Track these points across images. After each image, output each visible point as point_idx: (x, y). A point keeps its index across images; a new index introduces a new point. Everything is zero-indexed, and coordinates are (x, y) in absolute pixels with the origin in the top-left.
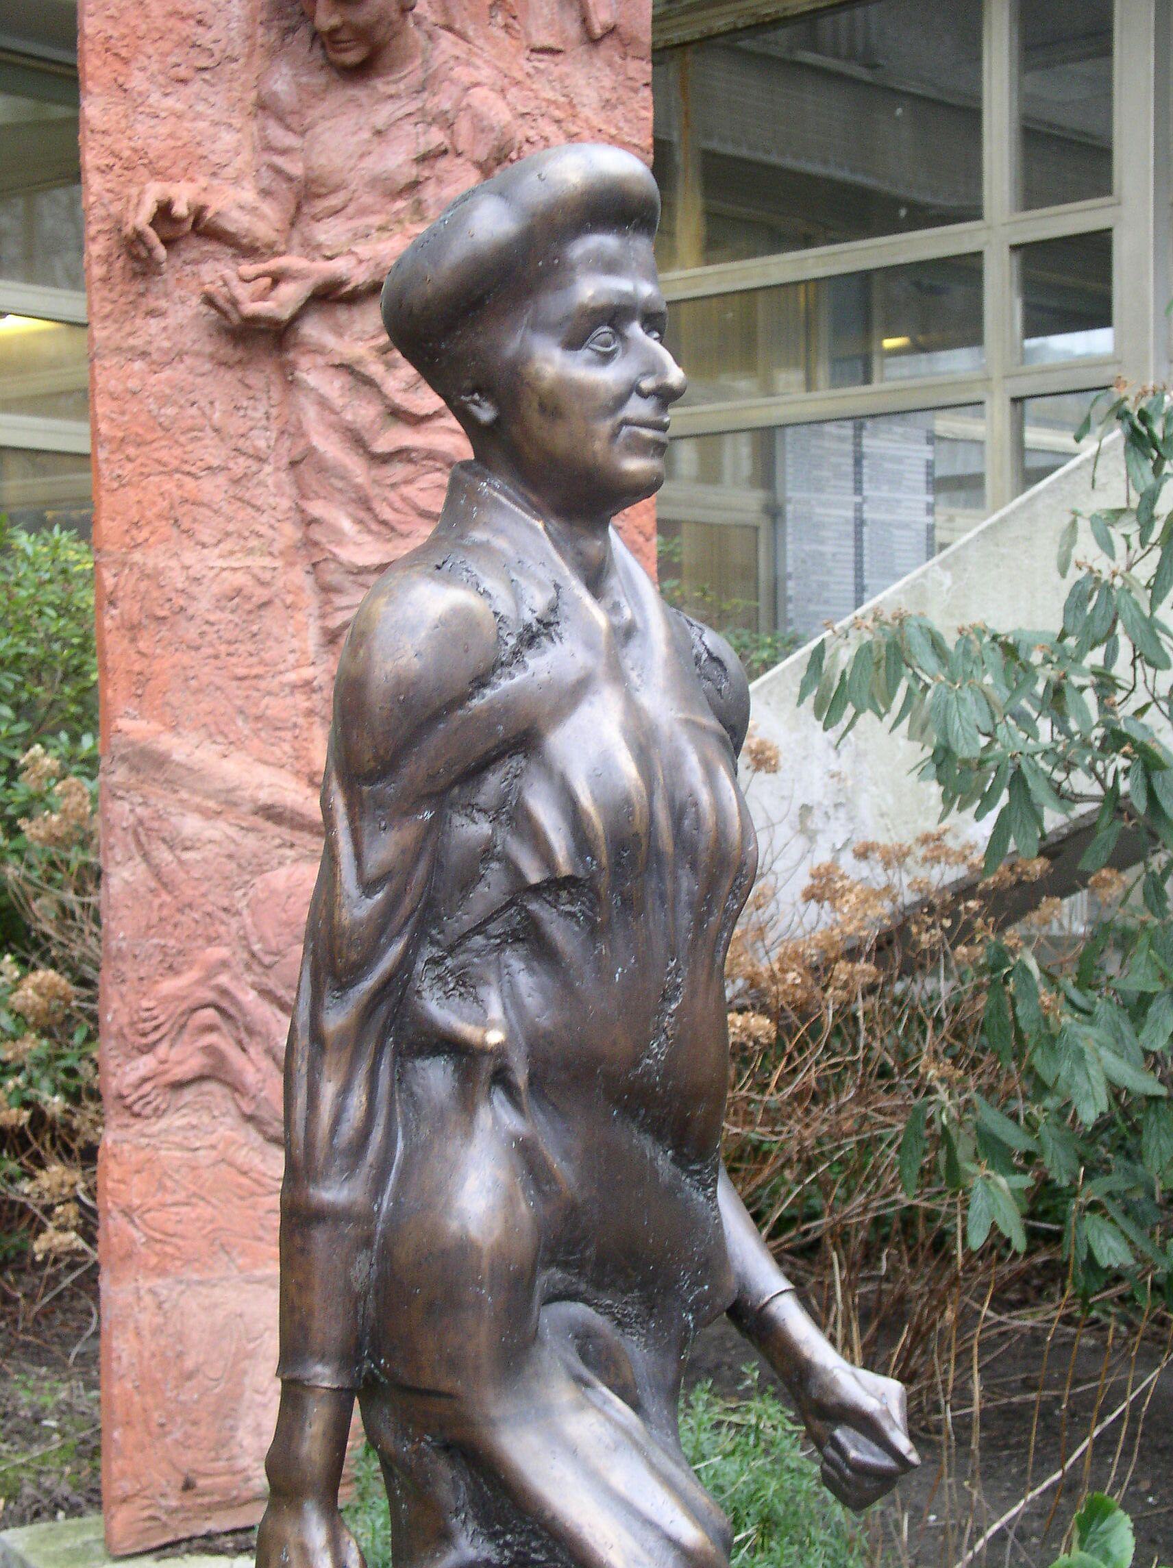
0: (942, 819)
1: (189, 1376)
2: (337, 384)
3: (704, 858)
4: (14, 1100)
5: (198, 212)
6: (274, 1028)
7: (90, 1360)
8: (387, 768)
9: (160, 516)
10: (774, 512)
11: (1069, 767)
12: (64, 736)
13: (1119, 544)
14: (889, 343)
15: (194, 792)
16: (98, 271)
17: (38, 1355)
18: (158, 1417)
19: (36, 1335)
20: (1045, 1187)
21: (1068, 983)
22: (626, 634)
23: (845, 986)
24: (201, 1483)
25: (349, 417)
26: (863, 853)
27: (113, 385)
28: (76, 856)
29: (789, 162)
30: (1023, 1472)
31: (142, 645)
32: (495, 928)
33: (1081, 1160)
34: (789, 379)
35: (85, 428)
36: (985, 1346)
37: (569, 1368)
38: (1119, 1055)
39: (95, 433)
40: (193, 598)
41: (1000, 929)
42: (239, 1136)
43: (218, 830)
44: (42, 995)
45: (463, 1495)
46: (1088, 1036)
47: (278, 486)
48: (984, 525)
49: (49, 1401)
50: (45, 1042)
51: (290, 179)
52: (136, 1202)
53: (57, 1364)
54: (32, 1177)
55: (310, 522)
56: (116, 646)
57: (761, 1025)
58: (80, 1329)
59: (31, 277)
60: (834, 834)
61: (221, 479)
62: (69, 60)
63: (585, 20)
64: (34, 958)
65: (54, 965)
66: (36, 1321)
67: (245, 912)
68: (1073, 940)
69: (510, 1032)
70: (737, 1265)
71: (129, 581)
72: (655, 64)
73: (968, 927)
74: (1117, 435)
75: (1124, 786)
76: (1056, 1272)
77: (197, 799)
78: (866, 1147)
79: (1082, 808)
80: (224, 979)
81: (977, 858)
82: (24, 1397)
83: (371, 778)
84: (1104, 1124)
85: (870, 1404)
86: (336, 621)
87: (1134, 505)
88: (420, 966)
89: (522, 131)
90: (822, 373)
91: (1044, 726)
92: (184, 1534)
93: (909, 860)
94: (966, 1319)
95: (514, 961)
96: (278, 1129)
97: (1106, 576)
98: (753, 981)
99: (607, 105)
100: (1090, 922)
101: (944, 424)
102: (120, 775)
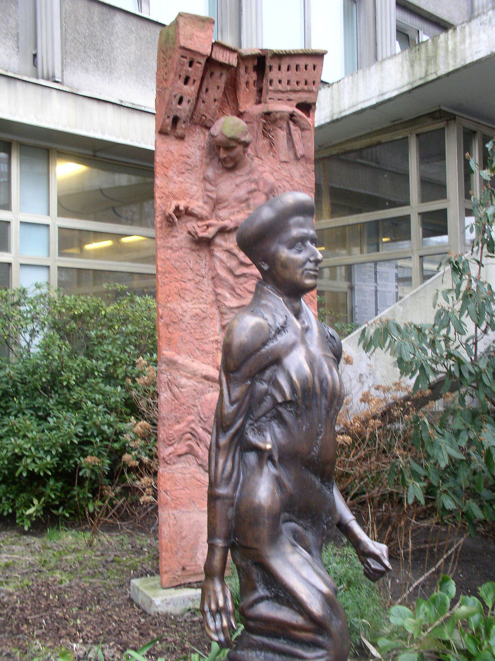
0: (400, 378)
1: (183, 538)
2: (225, 255)
3: (329, 395)
4: (135, 458)
5: (186, 209)
6: (207, 439)
7: (156, 532)
8: (237, 369)
9: (175, 293)
10: (352, 288)
11: (436, 363)
12: (148, 354)
13: (450, 299)
14: (384, 240)
15: (184, 371)
16: (158, 225)
17: (142, 530)
18: (175, 549)
19: (141, 524)
20: (430, 485)
21: (437, 427)
22: (306, 330)
23: (372, 427)
24: (187, 568)
25: (228, 264)
26: (377, 388)
27: (162, 257)
28: (152, 389)
29: (355, 190)
30: (424, 568)
31: (170, 330)
32: (268, 415)
33: (441, 478)
34: (356, 250)
35: (155, 267)
36: (413, 531)
37: (290, 542)
38: (451, 448)
39: (157, 269)
40: (184, 316)
41: (417, 410)
42: (197, 470)
43: (191, 382)
44: (142, 428)
45: (260, 577)
46: (443, 442)
47: (208, 284)
48: (412, 293)
49: (145, 544)
50: (143, 442)
51: (212, 198)
52: (168, 488)
53: (147, 533)
54: (140, 480)
55: (217, 294)
56: (162, 330)
57: (348, 439)
58: (153, 523)
59: (141, 225)
60: (369, 382)
61: (192, 283)
62: (151, 165)
63: (295, 154)
64: (140, 418)
65: (145, 420)
66: (141, 520)
67: (199, 407)
68: (438, 413)
69: (273, 445)
70: (339, 512)
71: (166, 311)
72: (315, 163)
73: (408, 409)
74: (449, 268)
75: (453, 369)
76: (434, 509)
77: (185, 374)
78: (378, 473)
79: (441, 375)
80: (193, 425)
81: (410, 389)
82: (138, 542)
83: (233, 372)
84: (447, 467)
85: (378, 552)
86: (224, 323)
87: (454, 288)
88: (247, 426)
89: (277, 184)
90: (365, 249)
91: (429, 351)
92: (182, 582)
93: (391, 391)
94: (408, 523)
95: (274, 424)
96: (207, 468)
97: (446, 309)
98: (345, 425)
99: (302, 176)
100: (444, 407)
101: (400, 263)
102: (164, 367)
